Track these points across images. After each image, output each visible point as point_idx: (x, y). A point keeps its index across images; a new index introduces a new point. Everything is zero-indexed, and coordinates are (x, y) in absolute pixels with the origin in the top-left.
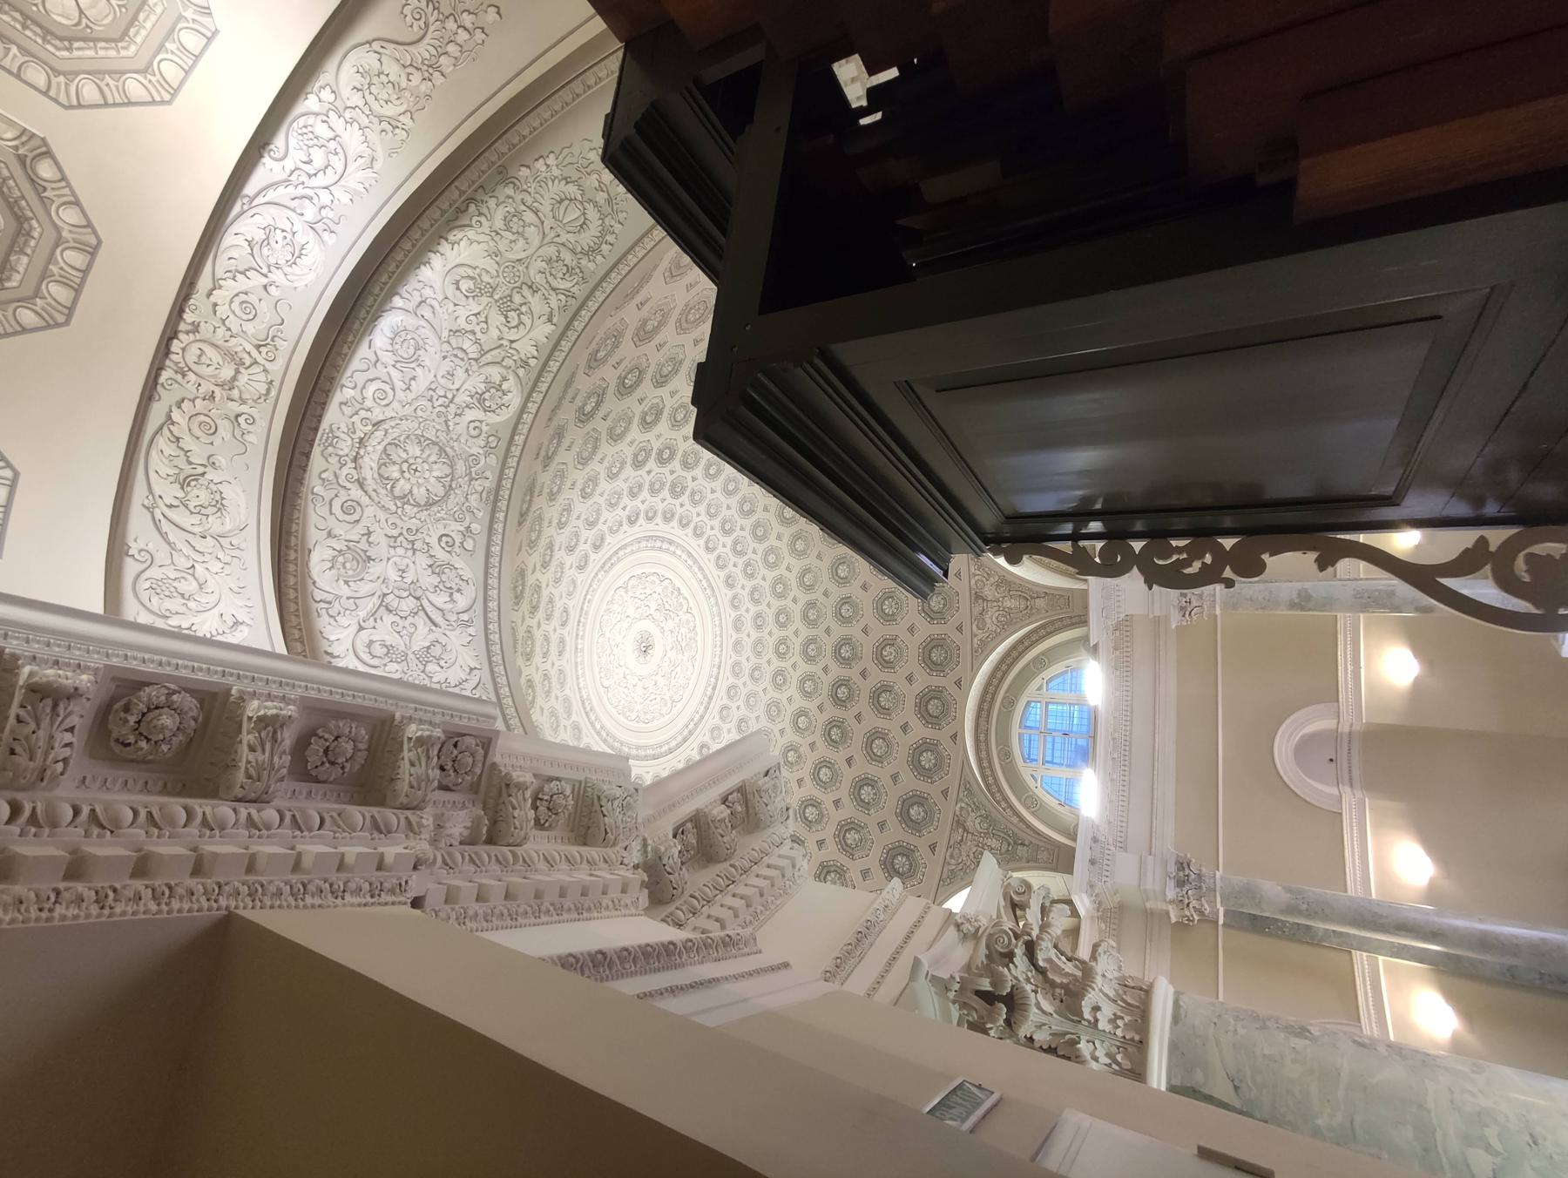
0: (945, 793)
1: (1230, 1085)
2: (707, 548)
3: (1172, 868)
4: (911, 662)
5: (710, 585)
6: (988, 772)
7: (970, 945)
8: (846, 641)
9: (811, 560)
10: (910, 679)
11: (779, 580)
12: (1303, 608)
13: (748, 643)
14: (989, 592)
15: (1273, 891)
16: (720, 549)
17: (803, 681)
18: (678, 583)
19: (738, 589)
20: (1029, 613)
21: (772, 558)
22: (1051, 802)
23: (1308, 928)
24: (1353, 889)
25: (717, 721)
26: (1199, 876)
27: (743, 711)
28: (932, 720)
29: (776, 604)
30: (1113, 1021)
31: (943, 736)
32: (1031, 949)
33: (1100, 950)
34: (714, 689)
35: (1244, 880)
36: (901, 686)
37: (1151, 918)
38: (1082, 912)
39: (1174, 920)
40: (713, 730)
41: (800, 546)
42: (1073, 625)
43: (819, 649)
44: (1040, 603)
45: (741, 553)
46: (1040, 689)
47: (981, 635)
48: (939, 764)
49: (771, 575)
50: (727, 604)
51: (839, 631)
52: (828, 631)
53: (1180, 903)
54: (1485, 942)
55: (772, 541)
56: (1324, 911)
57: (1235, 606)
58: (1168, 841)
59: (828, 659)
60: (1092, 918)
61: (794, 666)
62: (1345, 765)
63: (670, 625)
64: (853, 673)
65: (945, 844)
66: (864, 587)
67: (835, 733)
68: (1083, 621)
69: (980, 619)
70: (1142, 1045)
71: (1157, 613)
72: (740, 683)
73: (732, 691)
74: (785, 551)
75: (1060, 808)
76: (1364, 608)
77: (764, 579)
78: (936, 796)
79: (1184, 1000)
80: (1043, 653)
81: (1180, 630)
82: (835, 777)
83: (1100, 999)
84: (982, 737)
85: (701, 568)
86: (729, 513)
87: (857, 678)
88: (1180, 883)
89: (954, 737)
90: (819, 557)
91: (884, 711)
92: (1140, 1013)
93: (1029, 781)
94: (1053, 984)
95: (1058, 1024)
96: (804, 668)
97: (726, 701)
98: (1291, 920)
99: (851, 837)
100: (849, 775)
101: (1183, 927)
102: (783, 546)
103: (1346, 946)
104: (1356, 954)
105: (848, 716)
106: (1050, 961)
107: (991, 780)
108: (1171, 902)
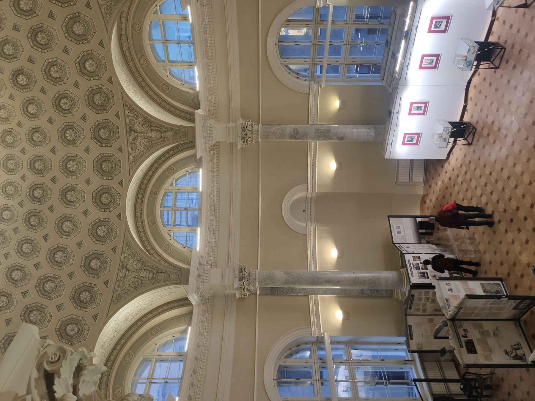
0: (114, 250)
3: (237, 272)
4: (88, 170)
10: (88, 182)
12: (295, 138)
14: (138, 127)
15: (279, 274)
20: (163, 141)
22: (179, 247)
23: (293, 288)
24: (310, 268)
28: (104, 207)
31: (112, 216)
36: (81, 186)
37: (228, 298)
38: (194, 303)
39: (238, 297)
42: (189, 148)
44: (169, 134)
46: (172, 184)
47: (134, 153)
48: (109, 233)
52: (23, 151)
53: (241, 289)
54: (356, 282)
56: (299, 280)
57: (267, 137)
59: (25, 170)
60: (199, 304)
62: (309, 212)
66: (50, 121)
68: (192, 145)
71: (231, 141)
76: (319, 138)
80: (173, 164)
81: (243, 150)
82: (35, 249)
84: (139, 214)
88: (241, 279)
89: (119, 216)
93: (167, 237)
100: (45, 247)
103: (306, 293)
104: (310, 296)
108: (237, 289)
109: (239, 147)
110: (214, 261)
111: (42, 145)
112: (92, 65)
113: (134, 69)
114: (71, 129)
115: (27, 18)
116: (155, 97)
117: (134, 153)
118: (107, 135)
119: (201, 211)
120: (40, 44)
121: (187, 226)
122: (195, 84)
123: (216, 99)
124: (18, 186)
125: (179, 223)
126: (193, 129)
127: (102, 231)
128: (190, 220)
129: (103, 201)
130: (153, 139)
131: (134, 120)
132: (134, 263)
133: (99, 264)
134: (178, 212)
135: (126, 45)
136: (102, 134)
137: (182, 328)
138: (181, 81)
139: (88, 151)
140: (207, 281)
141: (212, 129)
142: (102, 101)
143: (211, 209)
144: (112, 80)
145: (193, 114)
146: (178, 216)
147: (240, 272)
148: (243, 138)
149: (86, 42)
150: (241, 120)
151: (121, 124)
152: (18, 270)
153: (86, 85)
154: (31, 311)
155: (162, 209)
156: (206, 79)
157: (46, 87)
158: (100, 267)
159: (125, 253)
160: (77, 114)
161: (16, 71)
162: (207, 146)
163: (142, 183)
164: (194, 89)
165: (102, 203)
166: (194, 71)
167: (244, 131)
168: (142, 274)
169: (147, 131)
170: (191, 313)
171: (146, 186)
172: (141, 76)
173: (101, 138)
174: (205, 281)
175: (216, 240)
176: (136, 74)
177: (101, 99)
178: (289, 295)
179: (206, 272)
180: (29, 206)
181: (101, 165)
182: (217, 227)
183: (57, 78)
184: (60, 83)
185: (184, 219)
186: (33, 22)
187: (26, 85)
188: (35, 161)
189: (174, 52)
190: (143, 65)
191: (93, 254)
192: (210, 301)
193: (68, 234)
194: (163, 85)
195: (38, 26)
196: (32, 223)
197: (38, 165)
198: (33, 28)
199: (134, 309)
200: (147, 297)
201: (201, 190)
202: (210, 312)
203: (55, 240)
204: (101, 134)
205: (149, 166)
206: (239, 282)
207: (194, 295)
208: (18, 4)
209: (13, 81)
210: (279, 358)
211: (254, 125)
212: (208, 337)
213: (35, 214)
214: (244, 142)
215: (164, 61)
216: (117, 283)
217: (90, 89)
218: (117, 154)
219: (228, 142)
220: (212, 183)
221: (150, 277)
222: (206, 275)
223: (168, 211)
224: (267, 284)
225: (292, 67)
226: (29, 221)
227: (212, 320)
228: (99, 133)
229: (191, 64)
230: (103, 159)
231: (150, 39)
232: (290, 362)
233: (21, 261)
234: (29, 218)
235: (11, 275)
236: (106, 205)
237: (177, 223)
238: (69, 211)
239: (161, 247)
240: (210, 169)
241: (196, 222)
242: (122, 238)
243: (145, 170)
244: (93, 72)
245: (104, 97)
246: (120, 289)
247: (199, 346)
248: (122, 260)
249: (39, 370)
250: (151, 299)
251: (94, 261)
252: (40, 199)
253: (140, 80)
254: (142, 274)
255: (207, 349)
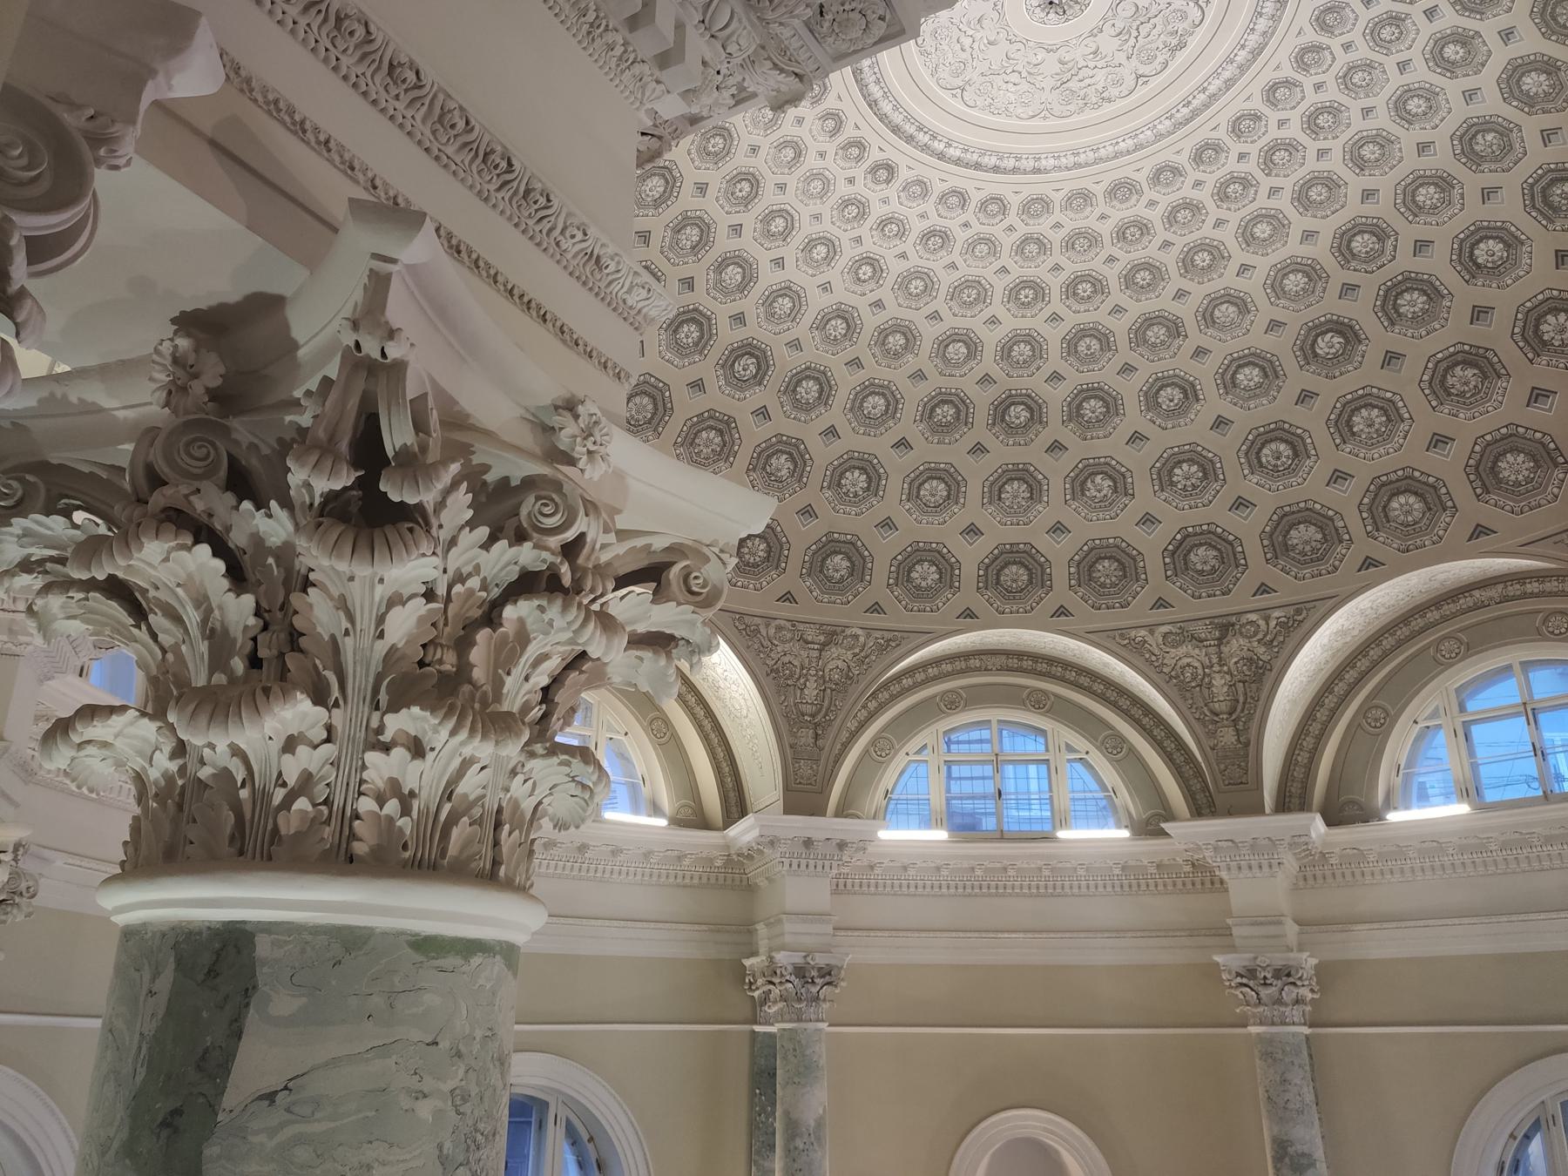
0: (876, 608)
1: (274, 1082)
2: (1274, 88)
3: (821, 960)
4: (1088, 527)
5: (1195, 114)
6: (920, 677)
7: (528, 439)
8: (1112, 405)
9: (1265, 310)
10: (1058, 528)
11: (1217, 253)
13: (1087, 219)
14: (1236, 646)
15: (815, 1102)
16: (1273, 116)
17: (1029, 339)
18: (1194, 43)
19: (1193, 175)
20: (1204, 721)
21: (1262, 230)
22: (888, 779)
23: (772, 1147)
25: (938, 188)
26: (816, 999)
27: (961, 236)
28: (992, 573)
29: (1170, 259)
30: (394, 787)
31: (968, 595)
32: (526, 584)
33: (577, 765)
34: (996, 169)
35: (823, 1062)
36: (1046, 514)
37: (743, 931)
38: (733, 831)
39: (747, 962)
40: (920, 183)
41: (1294, 282)
43: (1091, 358)
44: (1228, 736)
45: (1268, 164)
46: (1070, 749)
47: (1154, 641)
48: (920, 594)
49: (1228, 237)
50: (1159, 159)
51: (1130, 390)
52: (1127, 369)
53: (772, 971)
55: (1300, 222)
57: (1267, 1055)
58: (853, 954)
60: (727, 847)
61: (1055, 318)
63: (1107, 43)
64: (1055, 428)
65: (801, 617)
67: (945, 414)
68: (1203, 807)
69: (1183, 635)
70: (341, 857)
71: (1235, 931)
72: (1012, 218)
73: (995, 205)
74: (1279, 254)
75: (880, 793)
77: (1219, 223)
78: (869, 595)
79: (490, 970)
80: (1132, 751)
82: (872, 423)
83: (442, 759)
85: (1229, 83)
86: (1355, 115)
87: (1046, 437)
88: (800, 971)
89: (969, 614)
90: (1274, 325)
91: (995, 492)
92: (422, 856)
94: (463, 644)
95: (363, 656)
96: (1054, 336)
97: (976, 198)
98: (778, 1125)
99: (782, 464)
100: (878, 445)
101: (740, 975)
102: (1293, 247)
105: (980, 431)
106: (523, 639)
107: (906, 682)
108: (771, 958)
109: (1218, 959)
110: (849, 886)
111: (1148, 410)
112: (1407, 512)
113: (1418, 623)
114: (1205, 474)
115: (1518, 338)
116: (1340, 688)
117: (1154, 641)
118: (1199, 567)
119: (992, 840)
120: (1444, 376)
121: (948, 800)
122: (1407, 808)
123: (1368, 877)
124: (1032, 369)
125: (955, 774)
126: (1258, 810)
127: (925, 574)
128: (968, 806)
129: (1006, 571)
130: (1206, 691)
131: (1256, 633)
132: (840, 663)
133: (837, 576)
134: (988, 770)
135: (1491, 598)
136: (1202, 556)
137: (666, 802)
138: (1410, 763)
139: (1148, 522)
140: (795, 866)
141: (1266, 869)
142: (1300, 547)
143: (1005, 869)
144: (1372, 569)
145: (1304, 806)
146: (977, 771)
147: (820, 969)
148: (1251, 973)
149: (1479, 491)
150: (1313, 961)
151: (1240, 599)
152: (821, 392)
153: (1346, 502)
154: (721, 433)
155: (994, 725)
156: (1431, 842)
157: (1318, 403)
158: (829, 579)
159: (868, 636)
160: (1251, 486)
161: (1351, 327)
162: (1208, 854)
163: (1067, 665)
164: (1389, 805)
165: (1003, 568)
166: (1447, 798)
167: (1278, 974)
168: (811, 684)
169: (1229, 672)
170: (703, 824)
171: (1071, 683)
172: (1400, 644)
173: (1189, 552)
174: (795, 863)
175: (912, 889)
176: (1404, 632)
177: (1306, 542)
178: (751, 1135)
179: (820, 863)
180: (982, 399)
181: (1109, 558)
182: (952, 891)
183: (1351, 428)
184: (1336, 435)
185: (967, 787)
186: (1508, 351)
187: (1316, 355)
188: (1102, 399)
189: (1502, 741)
190: (1438, 650)
191: (864, 558)
192: (736, 878)
193: (913, 494)
194: (1385, 710)
195: (1498, 366)
196: (939, 411)
197: (1092, 407)
198: (1490, 354)
199: (720, 671)
200: (749, 703)
201: (1062, 834)
202: (704, 880)
203: (897, 467)
204: (1201, 551)
205: (1121, 682)
206: (790, 969)
207: (755, 833)
208: (1555, 311)
209: (1321, 324)
210: (569, 1102)
211: (1301, 1007)
212: (639, 877)
213: (963, 415)
214: (1238, 975)
215: (1462, 709)
216: (788, 625)
217: (1331, 513)
218: (1146, 596)
219: (1229, 921)
220: (1087, 870)
221: (803, 708)
222: (812, 863)
223: (989, 741)
224: (785, 1058)
225: (1536, 1147)
226: (944, 402)
227: (685, 886)
228: (1201, 545)
229: (1472, 792)
230: (1127, 561)
231: (1527, 666)
232: (555, 1136)
233: (842, 396)
234: (951, 402)
235: (808, 378)
236: (998, 579)
237: (955, 769)
238: (974, 490)
239: (884, 729)
240: (1132, 863)
241: (965, 827)
242: (907, 627)
243: (1106, 672)
244: (1386, 516)
245: (1313, 550)
246: (772, 631)
247: (616, 852)
248: (848, 632)
249: (669, 549)
250: (744, 712)
251: (846, 564)
252: (1003, 420)
253: (1388, 642)
254: (811, 684)
255: (607, 875)
